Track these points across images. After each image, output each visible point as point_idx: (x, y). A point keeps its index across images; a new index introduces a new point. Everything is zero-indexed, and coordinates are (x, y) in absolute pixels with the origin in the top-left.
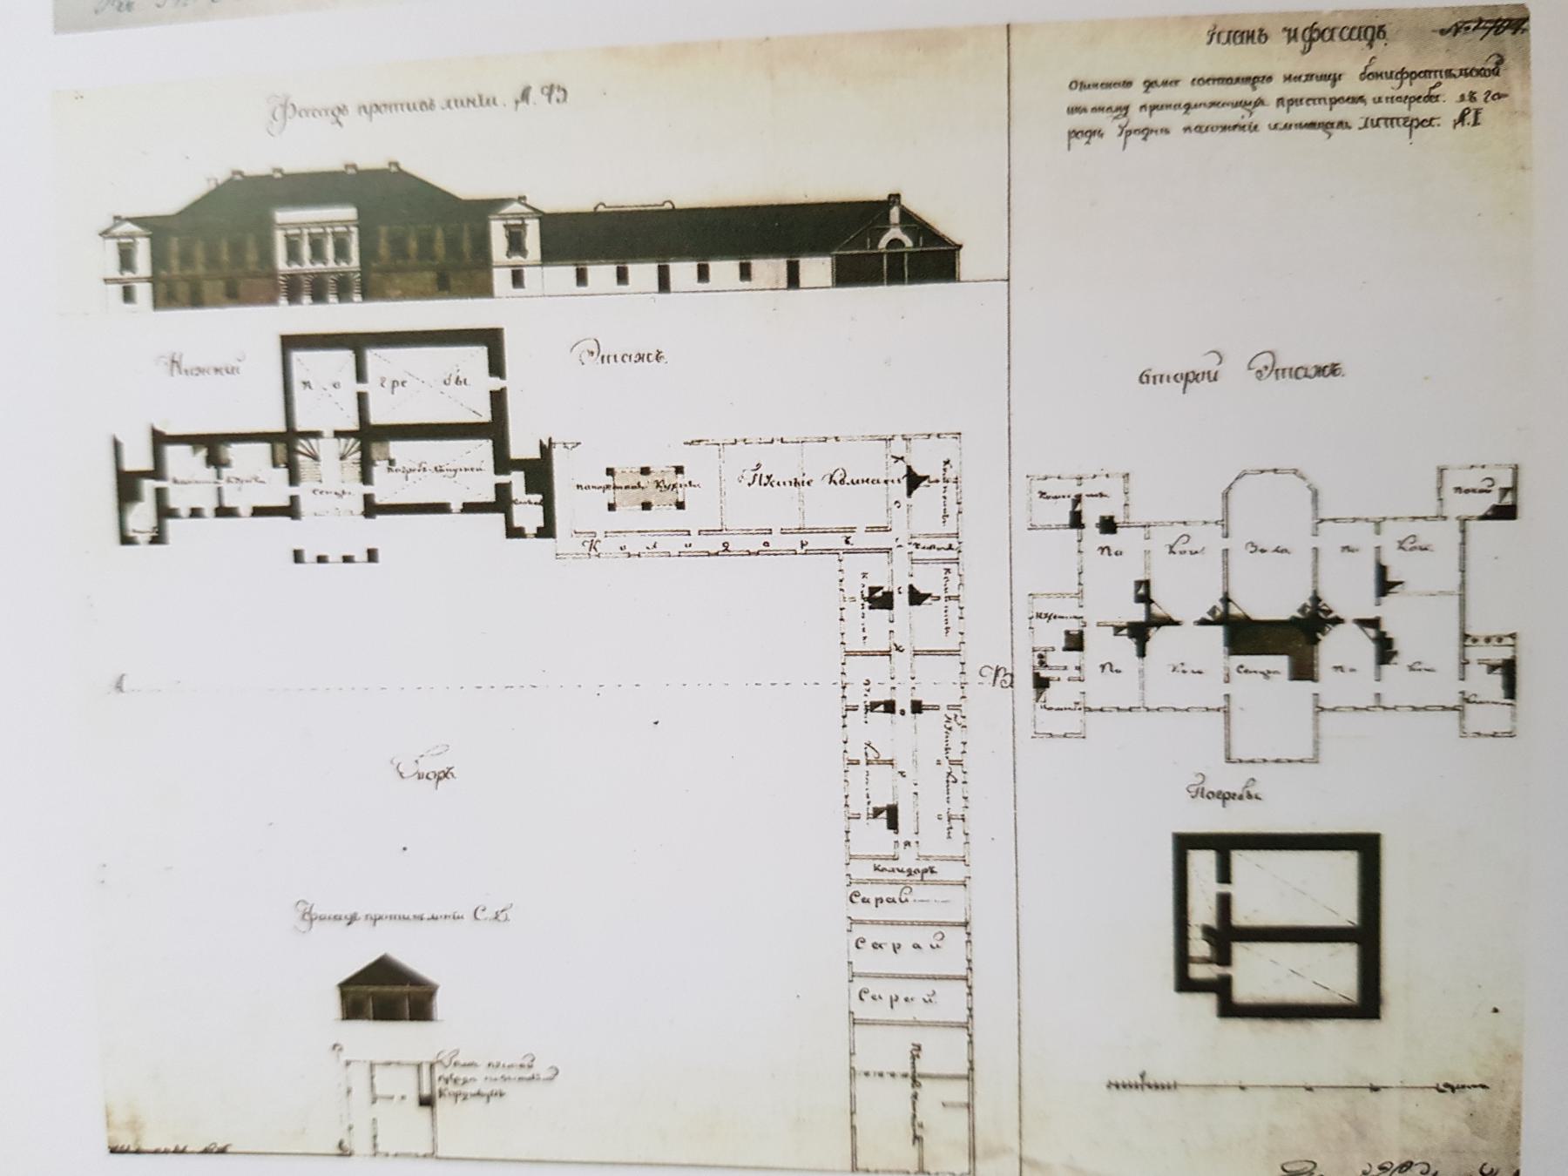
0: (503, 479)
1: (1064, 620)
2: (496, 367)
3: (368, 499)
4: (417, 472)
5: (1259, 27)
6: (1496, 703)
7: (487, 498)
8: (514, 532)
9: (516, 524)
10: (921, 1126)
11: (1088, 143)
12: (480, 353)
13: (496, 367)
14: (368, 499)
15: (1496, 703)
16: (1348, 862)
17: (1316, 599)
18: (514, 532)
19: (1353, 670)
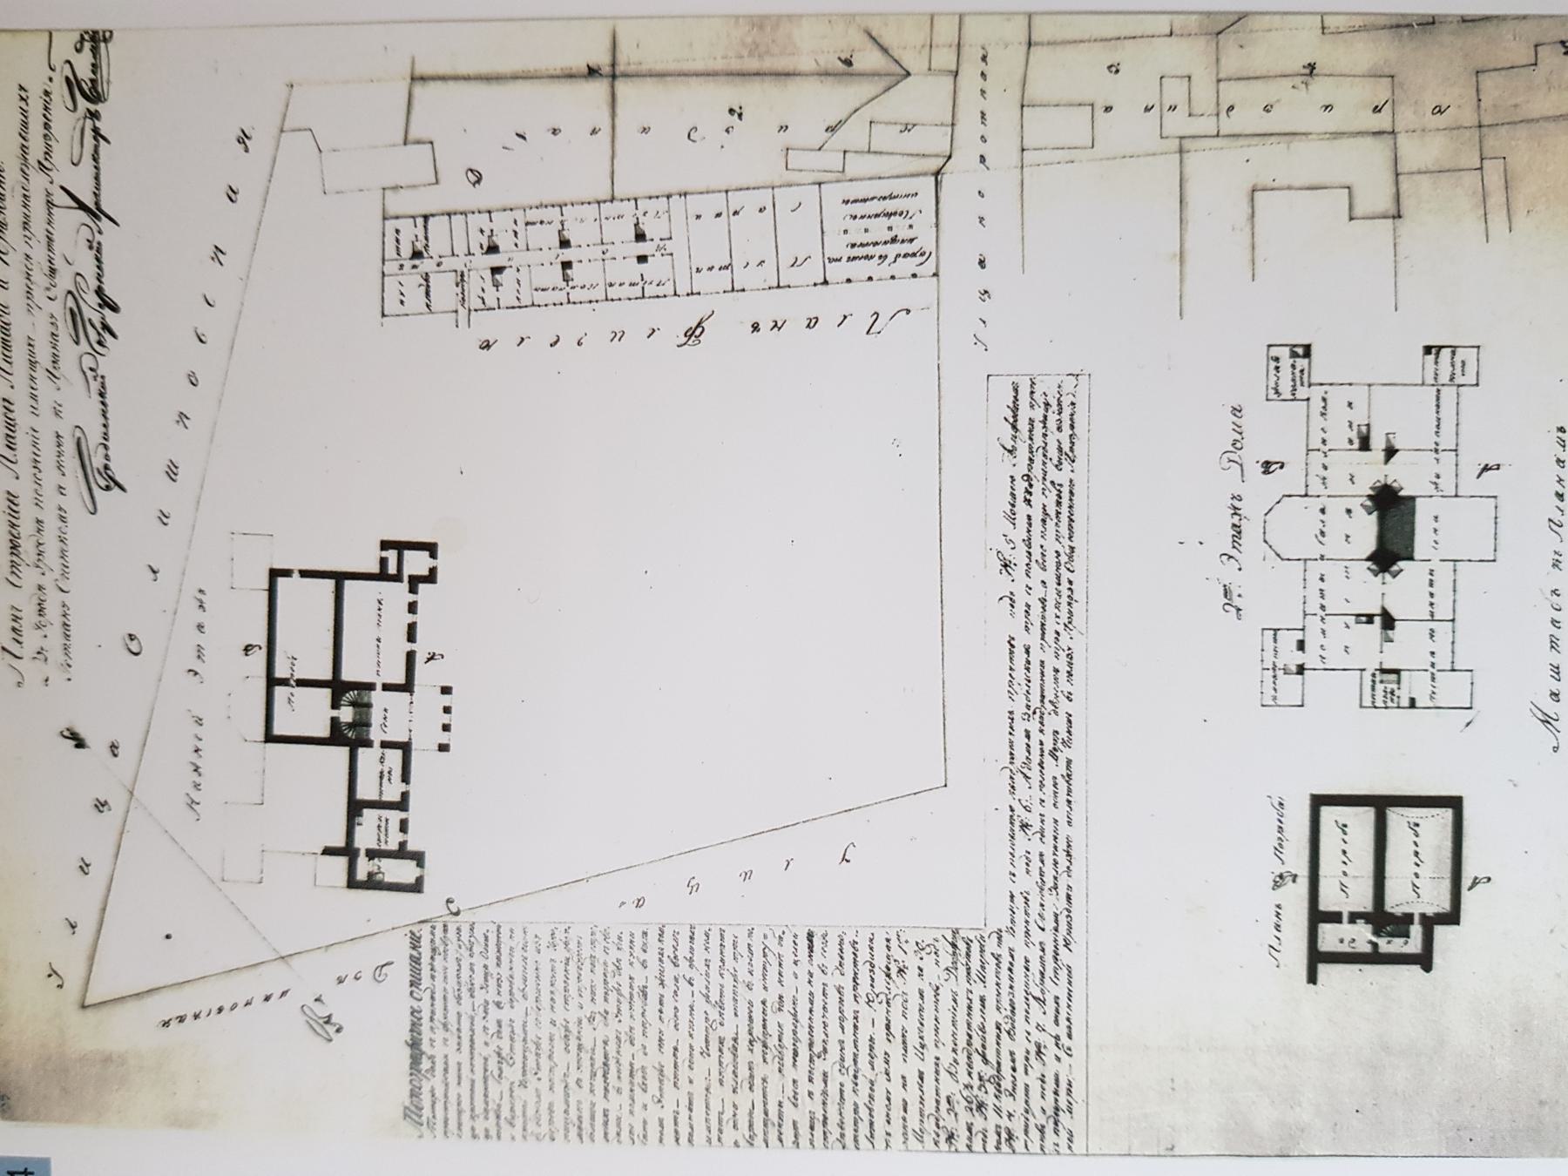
0: (384, 554)
1: (688, 260)
2: (287, 573)
3: (433, 555)
4: (538, 225)
5: (9, 610)
6: (513, 308)
7: (408, 562)
8: (431, 577)
9: (426, 573)
10: (906, 1032)
11: (656, 977)
12: (281, 581)
13: (287, 573)
14: (433, 555)
15: (513, 308)
16: (278, 730)
17: (1397, 451)
18: (431, 577)
19: (166, 1024)
